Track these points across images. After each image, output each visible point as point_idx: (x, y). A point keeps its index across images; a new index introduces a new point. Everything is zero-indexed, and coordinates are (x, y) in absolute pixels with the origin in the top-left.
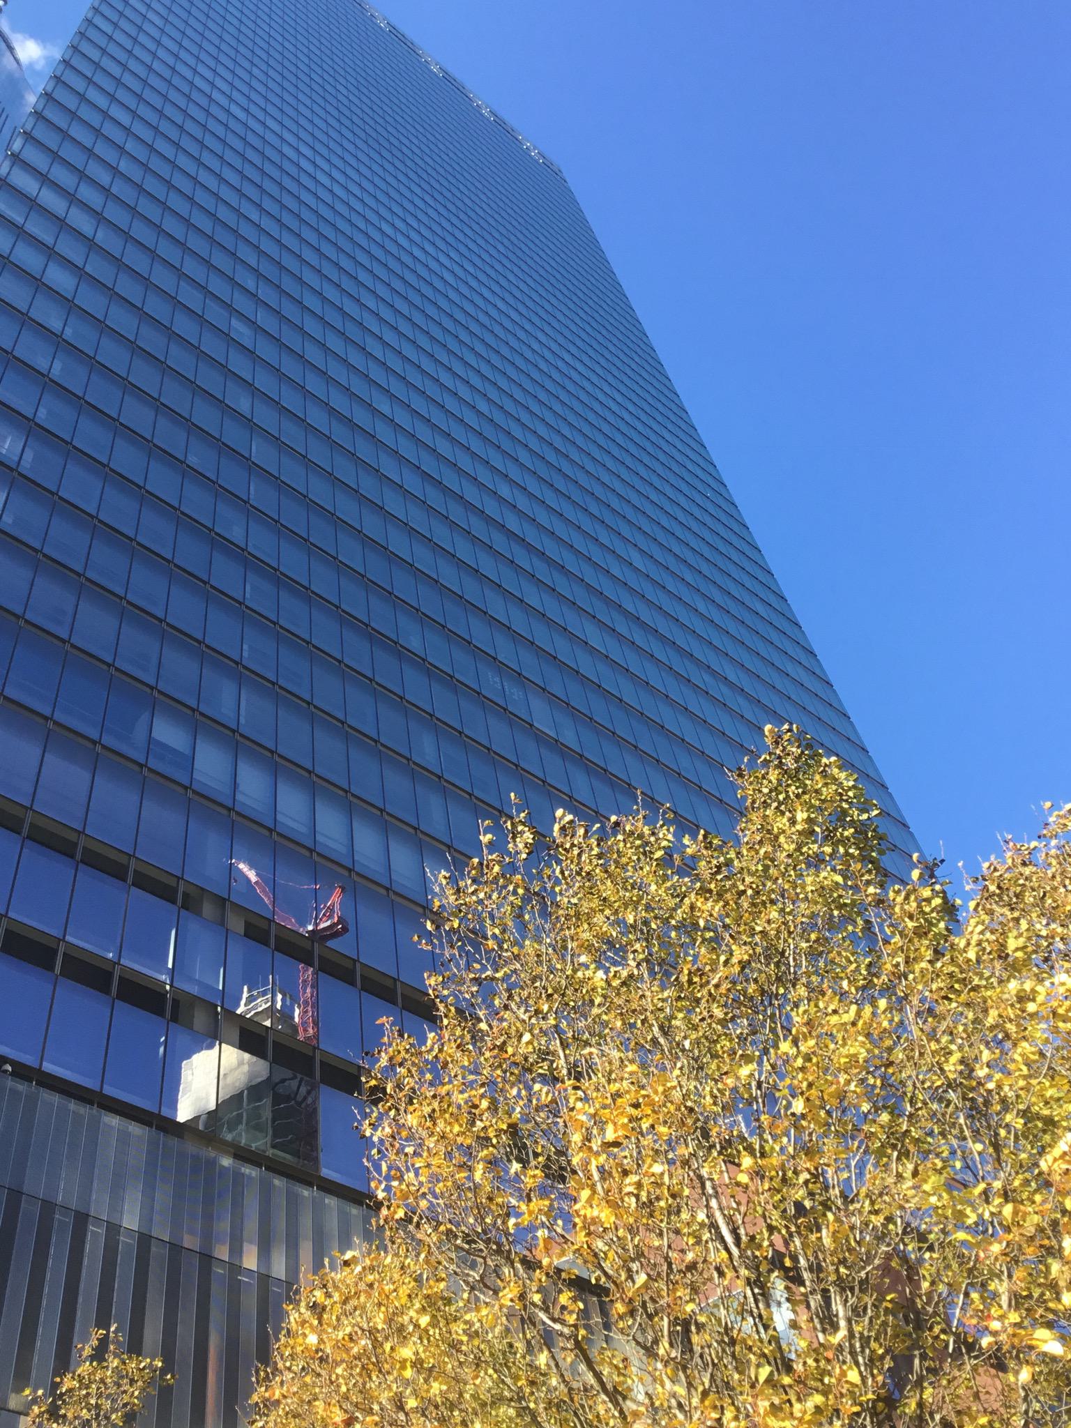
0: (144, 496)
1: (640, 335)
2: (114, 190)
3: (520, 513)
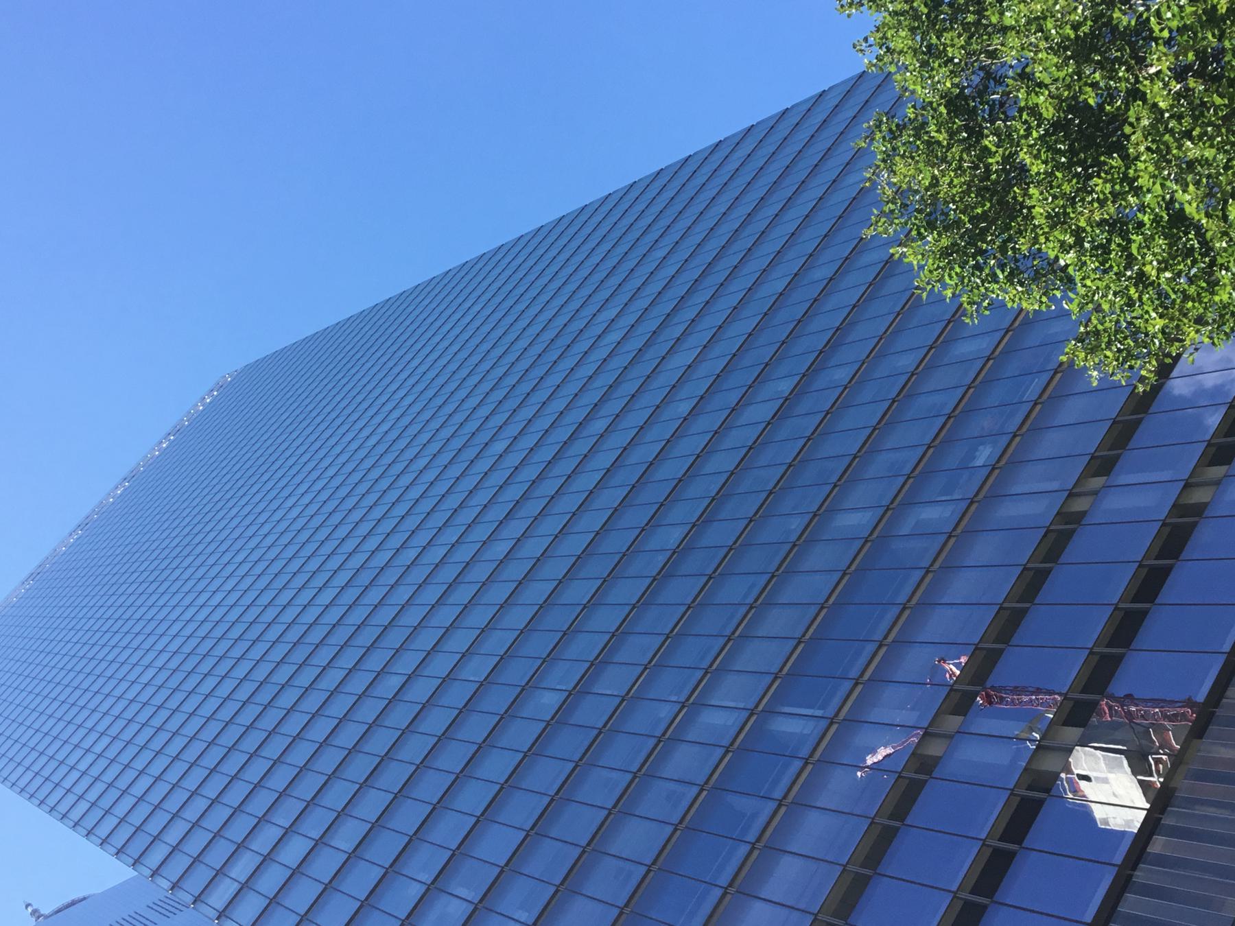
0: (509, 786)
1: (583, 218)
2: (316, 834)
3: (588, 419)
